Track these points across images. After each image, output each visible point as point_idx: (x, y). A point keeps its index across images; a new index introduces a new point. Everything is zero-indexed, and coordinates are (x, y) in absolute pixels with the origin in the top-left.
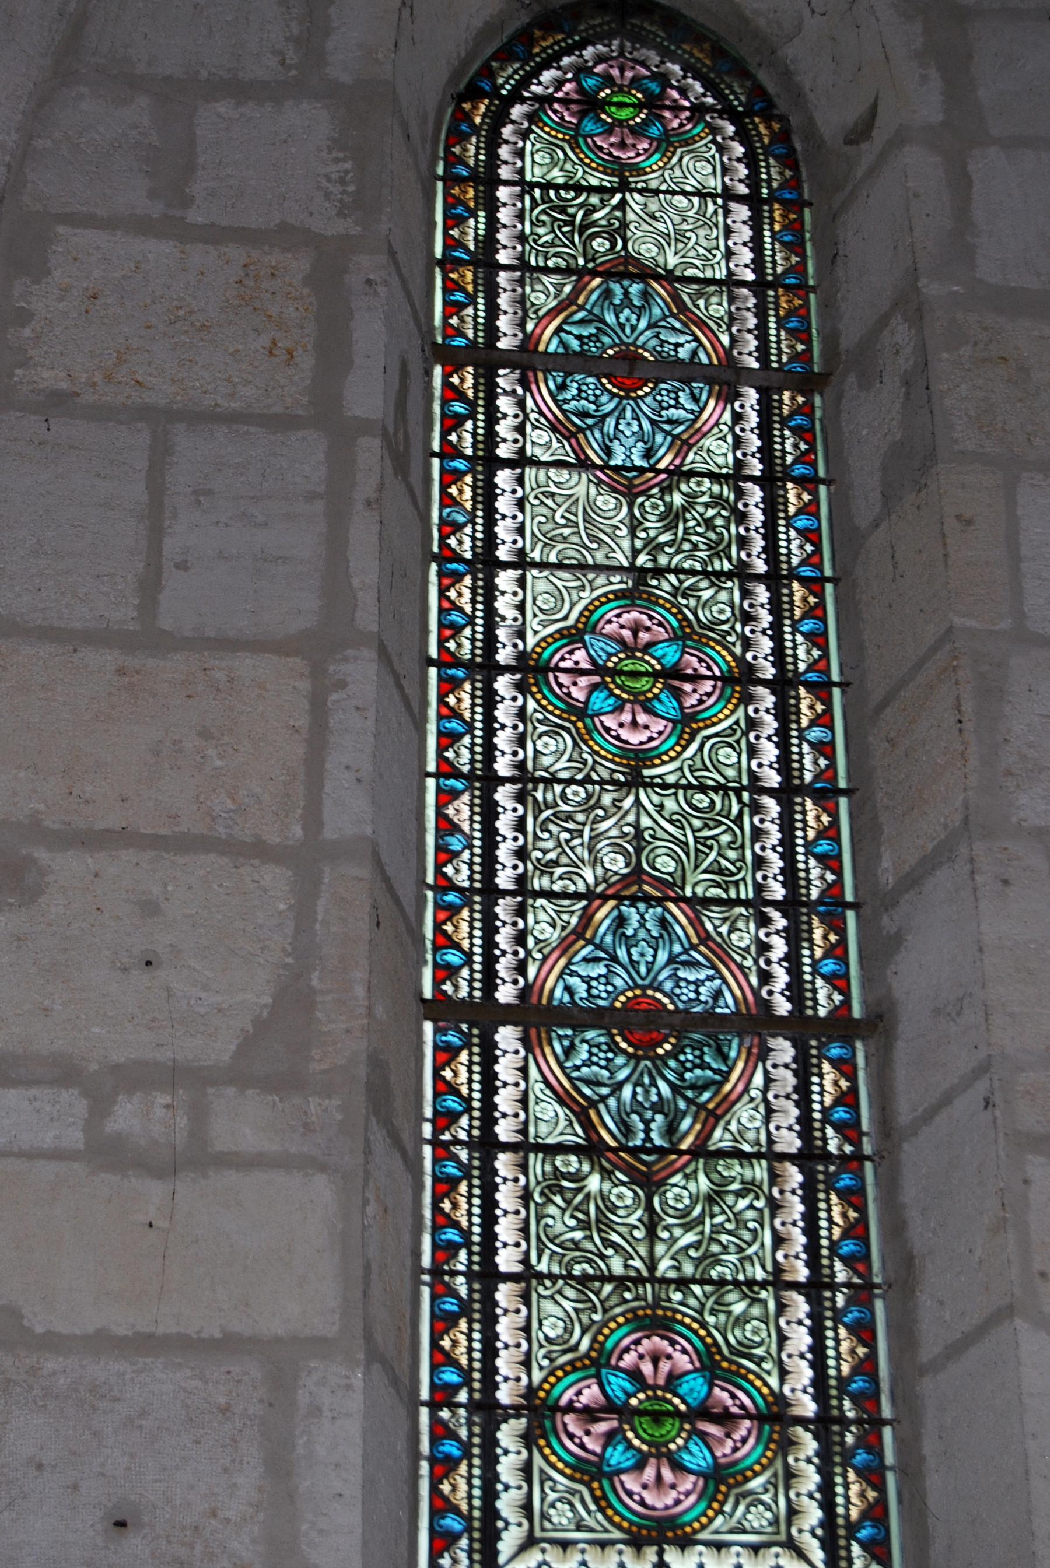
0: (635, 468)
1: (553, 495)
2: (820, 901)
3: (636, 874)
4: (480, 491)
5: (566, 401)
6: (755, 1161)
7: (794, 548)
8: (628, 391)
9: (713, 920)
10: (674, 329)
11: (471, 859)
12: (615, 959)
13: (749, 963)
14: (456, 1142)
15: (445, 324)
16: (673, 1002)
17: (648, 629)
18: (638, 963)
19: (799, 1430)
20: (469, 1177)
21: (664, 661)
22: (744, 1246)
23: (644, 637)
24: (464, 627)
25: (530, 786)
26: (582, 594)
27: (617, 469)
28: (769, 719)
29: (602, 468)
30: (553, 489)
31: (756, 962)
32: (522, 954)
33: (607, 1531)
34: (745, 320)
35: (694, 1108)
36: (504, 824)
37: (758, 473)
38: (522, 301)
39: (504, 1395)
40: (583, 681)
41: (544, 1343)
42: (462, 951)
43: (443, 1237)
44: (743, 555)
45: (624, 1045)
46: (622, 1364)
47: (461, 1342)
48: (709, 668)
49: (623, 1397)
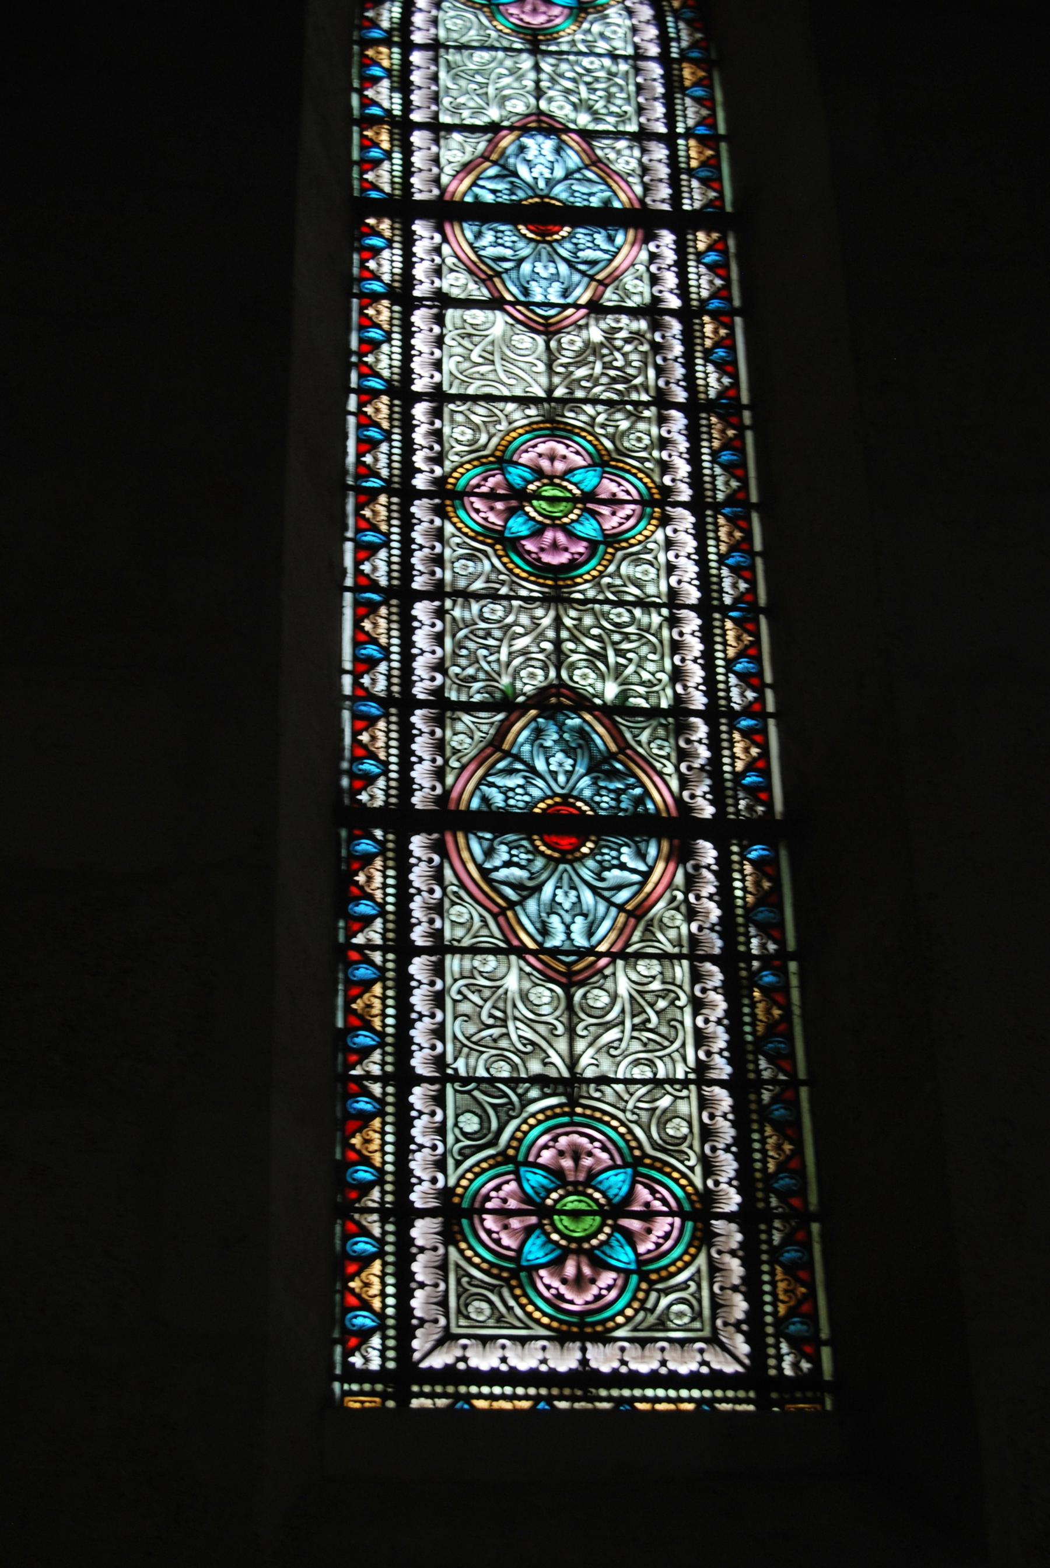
0: (553, 305)
1: (470, 335)
2: (732, 608)
3: (570, 980)
4: (397, 409)
5: (484, 248)
6: (676, 962)
7: (702, 283)
8: (543, 234)
9: (603, 149)
10: (589, 180)
11: (384, 994)
12: (533, 770)
13: (670, 769)
14: (369, 1076)
15: (359, 463)
16: (592, 809)
17: (590, 1154)
18: (556, 773)
19: (667, 318)
20: (382, 1114)
21: (582, 486)
22: (666, 1043)
23: (560, 466)
24: (381, 442)
25: (448, 604)
26: (498, 427)
27: (555, 952)
28: (718, 999)
29: (534, 953)
30: (470, 330)
31: (677, 769)
32: (440, 761)
33: (528, 1327)
34: (654, 89)
35: (586, 280)
36: (421, 638)
37: (717, 951)
38: (440, 746)
39: (418, 1198)
40: (515, 1223)
41: (461, 1137)
42: (372, 1030)
43: (363, 651)
44: (710, 1183)
45: (542, 848)
46: (540, 1160)
47: (380, 626)
48: (628, 492)
49: (522, 483)
